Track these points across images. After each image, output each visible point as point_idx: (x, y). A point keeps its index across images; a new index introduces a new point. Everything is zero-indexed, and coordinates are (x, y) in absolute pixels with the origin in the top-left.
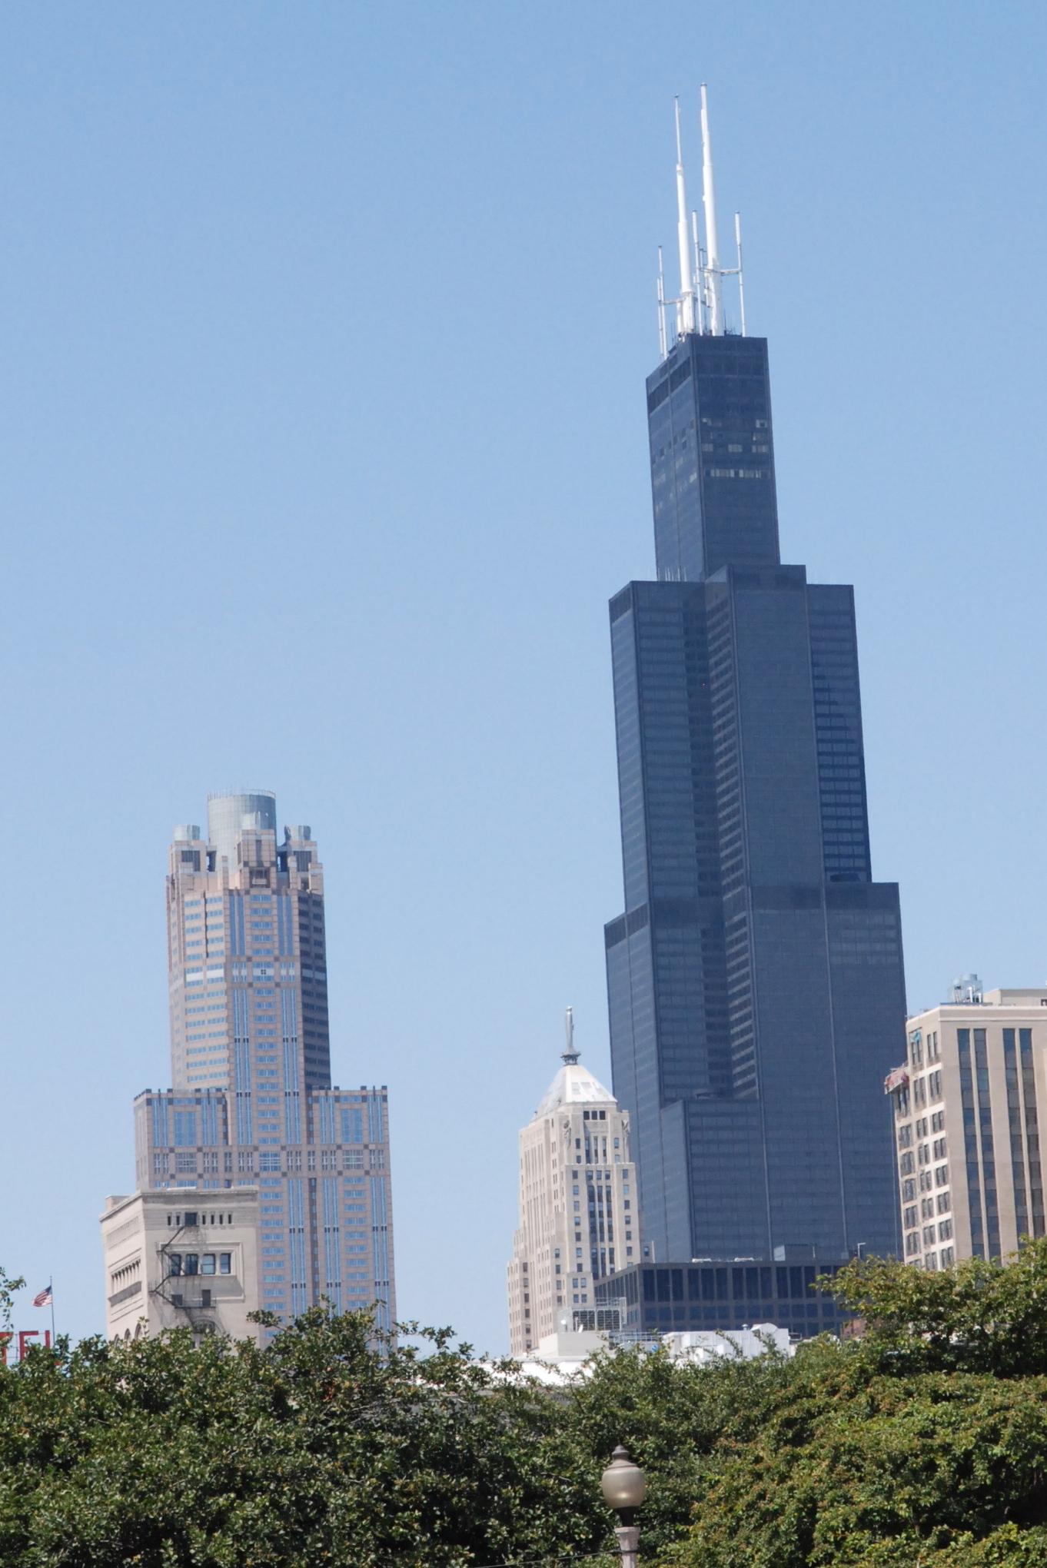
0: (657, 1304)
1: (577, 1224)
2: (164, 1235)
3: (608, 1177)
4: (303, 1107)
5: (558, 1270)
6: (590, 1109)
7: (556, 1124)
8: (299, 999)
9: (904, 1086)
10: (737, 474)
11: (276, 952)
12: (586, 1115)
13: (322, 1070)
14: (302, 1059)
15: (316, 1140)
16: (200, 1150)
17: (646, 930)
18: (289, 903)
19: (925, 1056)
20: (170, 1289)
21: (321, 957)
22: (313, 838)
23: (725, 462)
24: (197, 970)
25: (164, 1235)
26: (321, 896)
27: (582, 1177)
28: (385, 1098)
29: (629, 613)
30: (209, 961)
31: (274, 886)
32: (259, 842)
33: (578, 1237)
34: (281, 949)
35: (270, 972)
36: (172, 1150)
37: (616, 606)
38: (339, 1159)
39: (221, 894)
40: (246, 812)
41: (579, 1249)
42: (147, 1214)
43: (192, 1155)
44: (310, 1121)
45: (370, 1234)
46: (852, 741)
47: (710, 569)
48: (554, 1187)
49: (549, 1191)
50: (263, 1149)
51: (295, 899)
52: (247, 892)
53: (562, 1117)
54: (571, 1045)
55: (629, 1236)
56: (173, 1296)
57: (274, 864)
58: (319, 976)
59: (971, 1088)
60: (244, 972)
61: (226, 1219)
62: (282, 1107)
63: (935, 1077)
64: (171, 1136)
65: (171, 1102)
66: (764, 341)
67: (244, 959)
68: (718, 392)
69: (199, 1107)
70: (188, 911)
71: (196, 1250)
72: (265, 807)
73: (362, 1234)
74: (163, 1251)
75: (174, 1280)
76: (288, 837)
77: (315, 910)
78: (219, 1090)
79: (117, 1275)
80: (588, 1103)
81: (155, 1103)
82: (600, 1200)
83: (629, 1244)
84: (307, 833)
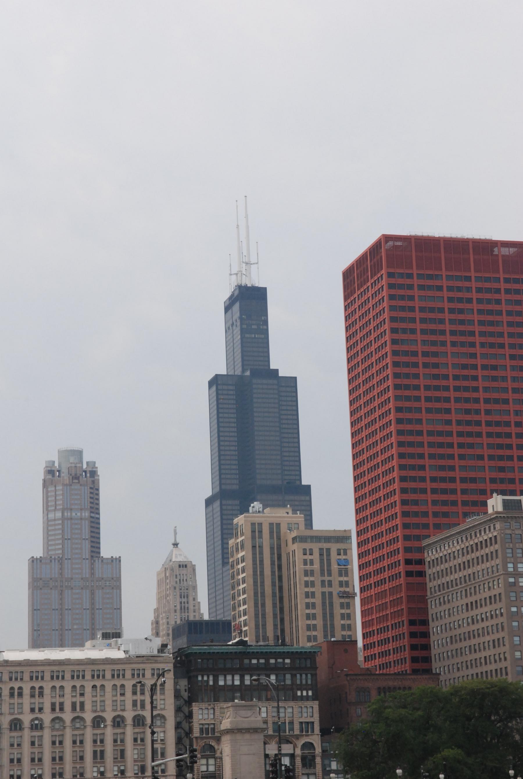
0: (118, 631)
5: (168, 623)
12: (180, 566)
19: (239, 533)
27: (178, 589)
28: (120, 561)
33: (175, 611)
37: (211, 383)
49: (166, 594)
54: (175, 540)
68: (249, 305)
77: (96, 492)
80: (180, 562)
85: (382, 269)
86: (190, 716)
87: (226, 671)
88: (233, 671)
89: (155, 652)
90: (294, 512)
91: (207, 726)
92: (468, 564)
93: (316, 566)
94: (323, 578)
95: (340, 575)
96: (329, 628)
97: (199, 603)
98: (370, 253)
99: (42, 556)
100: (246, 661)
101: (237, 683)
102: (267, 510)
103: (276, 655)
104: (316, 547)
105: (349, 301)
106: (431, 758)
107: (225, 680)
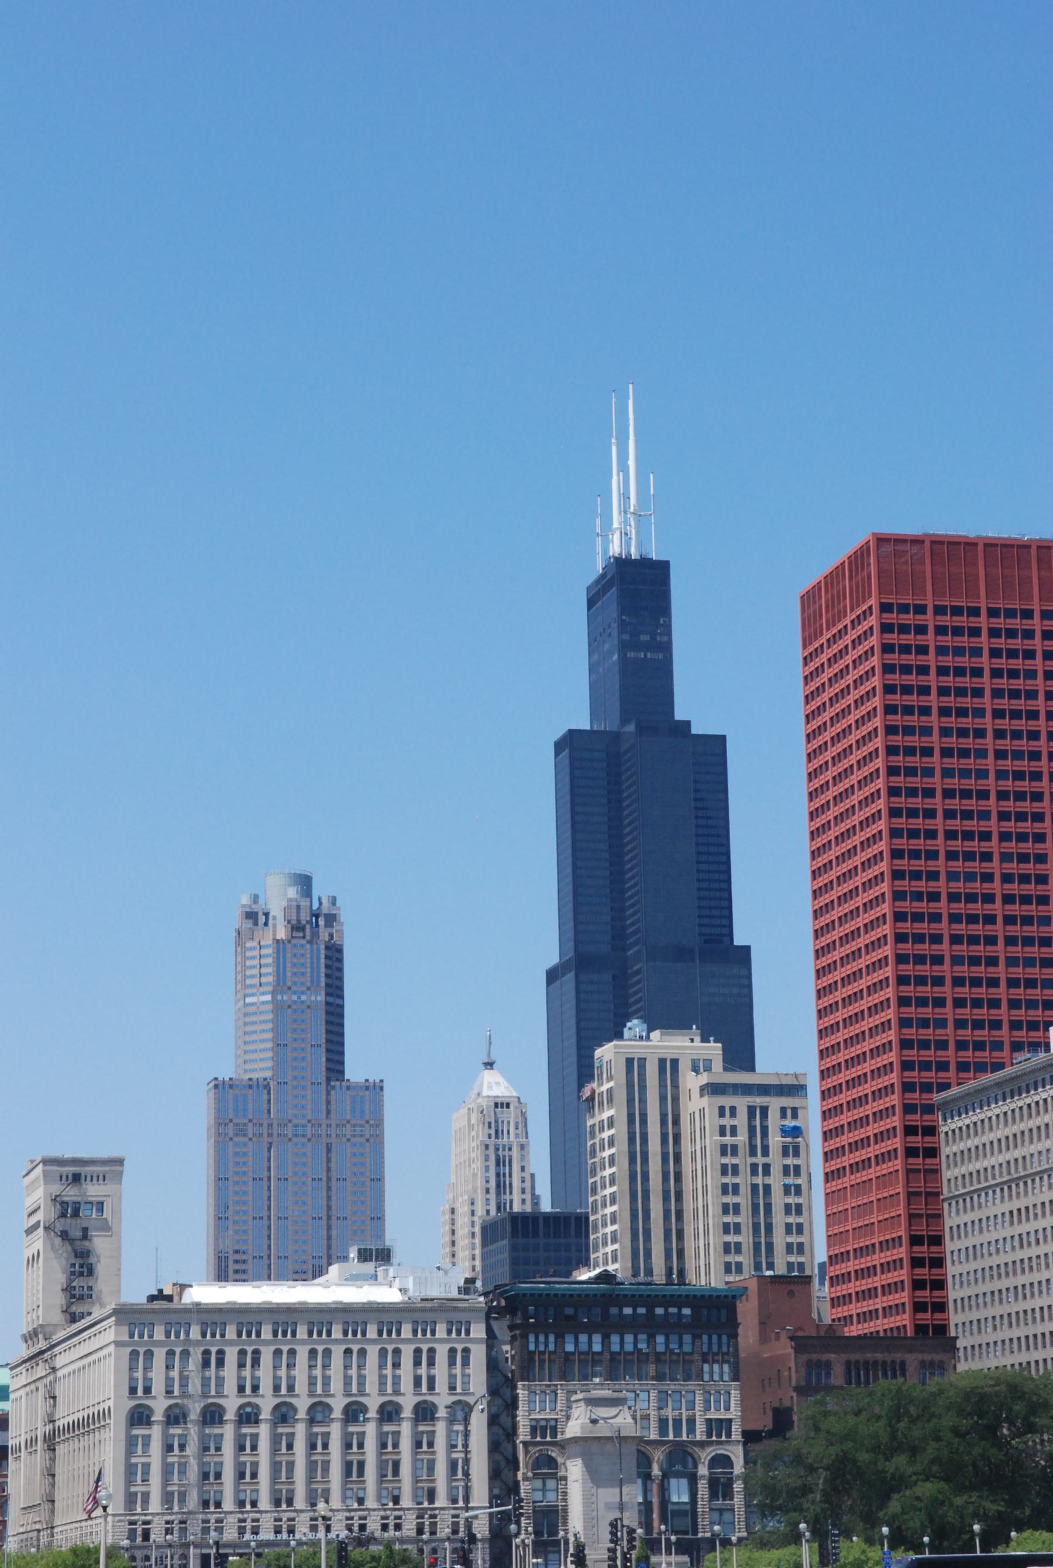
0: (521, 1241)
1: (487, 1182)
2: (56, 1188)
3: (510, 1149)
4: (324, 1092)
5: (473, 1213)
6: (499, 1101)
7: (475, 1111)
8: (324, 1017)
9: (591, 1099)
10: (645, 655)
11: (308, 984)
12: (496, 1105)
13: (338, 1067)
14: (324, 1059)
15: (333, 1116)
16: (250, 1121)
17: (571, 975)
18: (318, 950)
20: (59, 1227)
21: (341, 988)
22: (338, 903)
23: (637, 647)
24: (253, 995)
25: (56, 1188)
26: (342, 945)
27: (492, 1149)
28: (382, 1088)
29: (566, 752)
30: (262, 989)
31: (308, 937)
32: (298, 907)
33: (487, 1191)
34: (312, 982)
35: (304, 998)
36: (231, 1121)
37: (559, 746)
38: (348, 1130)
39: (270, 942)
40: (290, 885)
41: (488, 1199)
42: (45, 1174)
43: (245, 1124)
44: (328, 1102)
45: (368, 1183)
46: (723, 845)
47: (624, 721)
48: (473, 1155)
49: (469, 1158)
50: (295, 1121)
51: (323, 947)
52: (289, 942)
53: (480, 1106)
54: (489, 1055)
55: (523, 1191)
56: (62, 1232)
57: (308, 922)
58: (338, 1001)
59: (634, 1100)
60: (285, 998)
61: (101, 1178)
62: (309, 1092)
63: (610, 1091)
64: (231, 1111)
65: (231, 1087)
66: (668, 563)
67: (285, 989)
68: (635, 598)
69: (250, 1091)
70: (249, 954)
71: (78, 1199)
72: (305, 883)
73: (363, 1183)
74: (54, 1200)
75: (62, 1220)
76: (321, 903)
78: (265, 1079)
79: (31, 1214)
80: (498, 1097)
81: (221, 1087)
82: (504, 1165)
83: (524, 1196)
84: (333, 901)
85: (870, 596)
86: (512, 1405)
87: (577, 1328)
88: (590, 1329)
89: (455, 1294)
90: (704, 1040)
91: (543, 1423)
92: (1015, 1140)
93: (742, 1138)
94: (754, 1160)
95: (785, 1153)
96: (764, 1250)
97: (533, 1176)
98: (850, 563)
99: (233, 1076)
100: (614, 1311)
101: (597, 1348)
102: (655, 1035)
103: (667, 1301)
104: (741, 1103)
105: (811, 649)
106: (896, 1496)
107: (577, 1342)
